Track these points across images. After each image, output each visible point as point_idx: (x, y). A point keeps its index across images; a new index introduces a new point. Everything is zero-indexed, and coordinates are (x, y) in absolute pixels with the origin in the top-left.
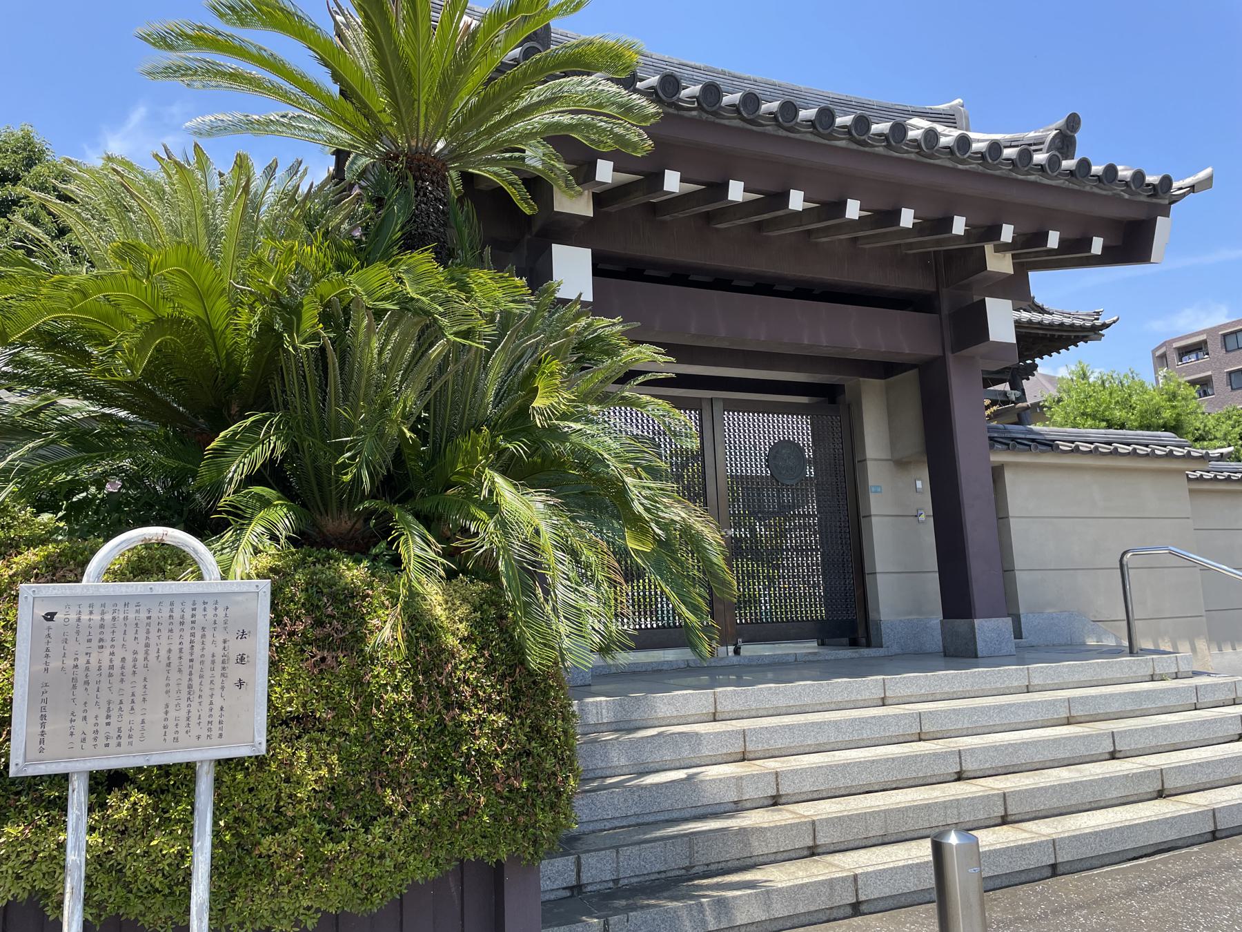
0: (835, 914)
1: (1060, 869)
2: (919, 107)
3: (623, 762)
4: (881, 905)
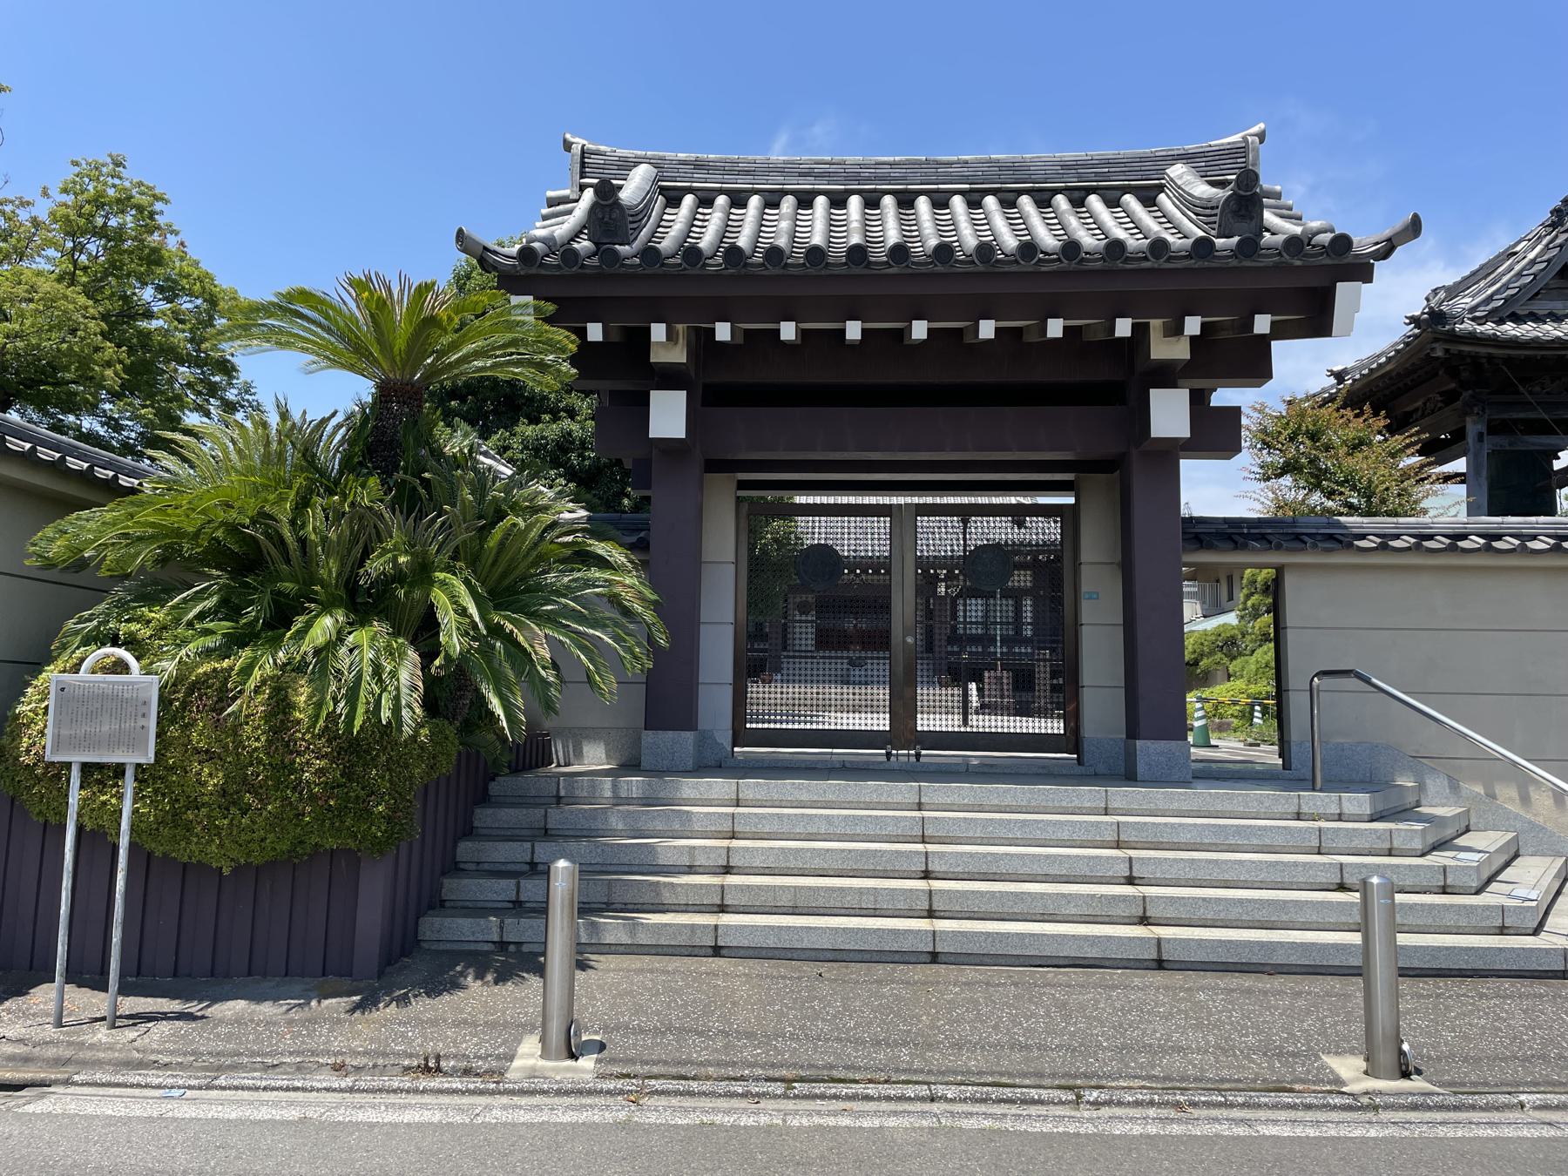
0: (696, 951)
1: (942, 958)
2: (1178, 148)
3: (620, 826)
4: (742, 953)
